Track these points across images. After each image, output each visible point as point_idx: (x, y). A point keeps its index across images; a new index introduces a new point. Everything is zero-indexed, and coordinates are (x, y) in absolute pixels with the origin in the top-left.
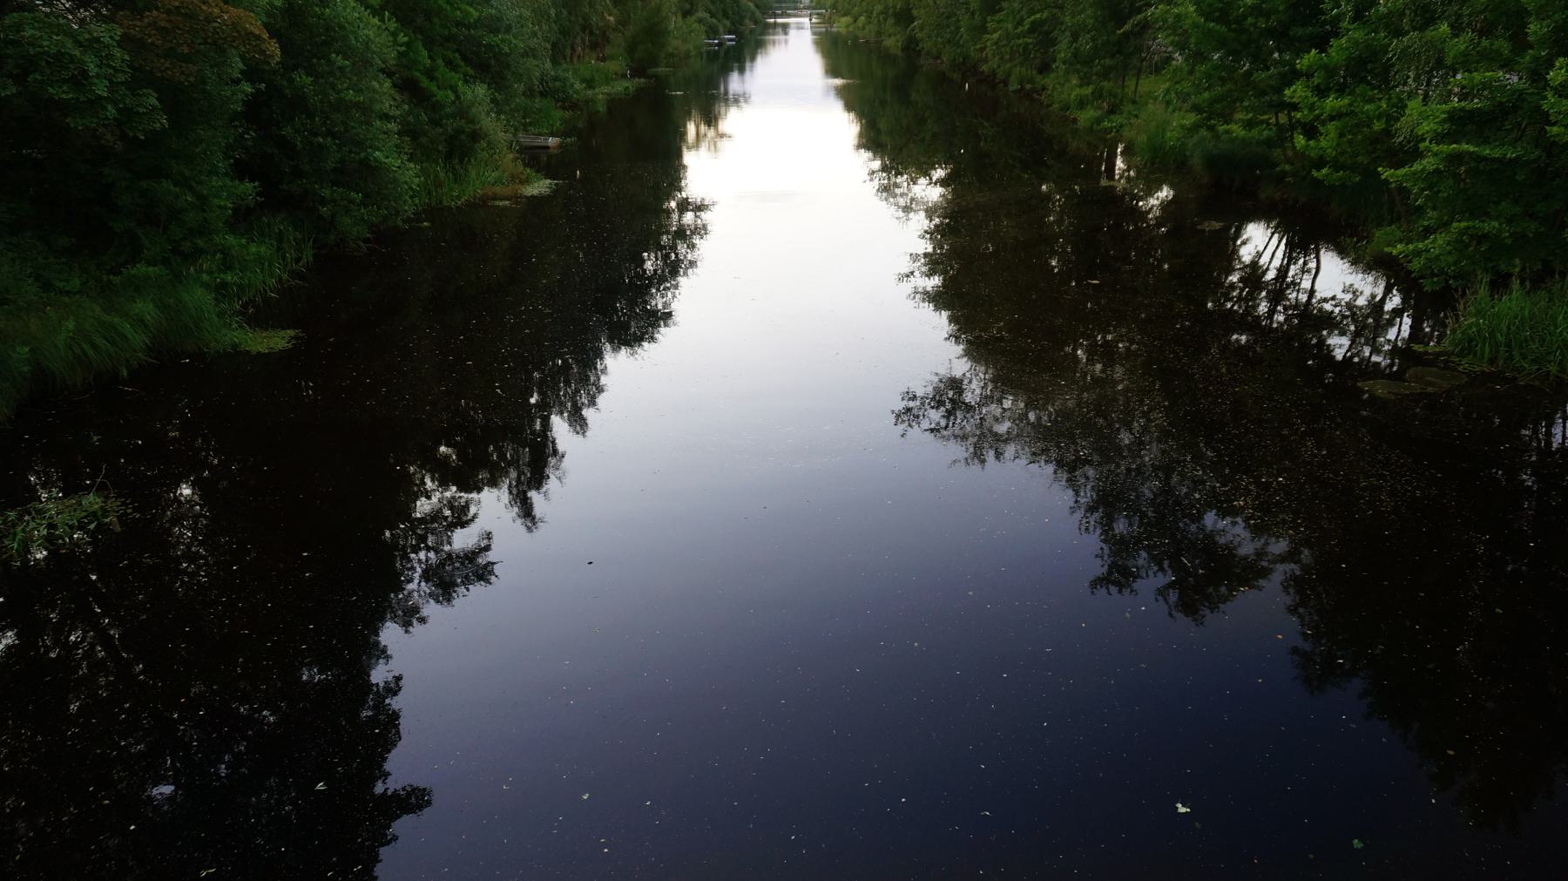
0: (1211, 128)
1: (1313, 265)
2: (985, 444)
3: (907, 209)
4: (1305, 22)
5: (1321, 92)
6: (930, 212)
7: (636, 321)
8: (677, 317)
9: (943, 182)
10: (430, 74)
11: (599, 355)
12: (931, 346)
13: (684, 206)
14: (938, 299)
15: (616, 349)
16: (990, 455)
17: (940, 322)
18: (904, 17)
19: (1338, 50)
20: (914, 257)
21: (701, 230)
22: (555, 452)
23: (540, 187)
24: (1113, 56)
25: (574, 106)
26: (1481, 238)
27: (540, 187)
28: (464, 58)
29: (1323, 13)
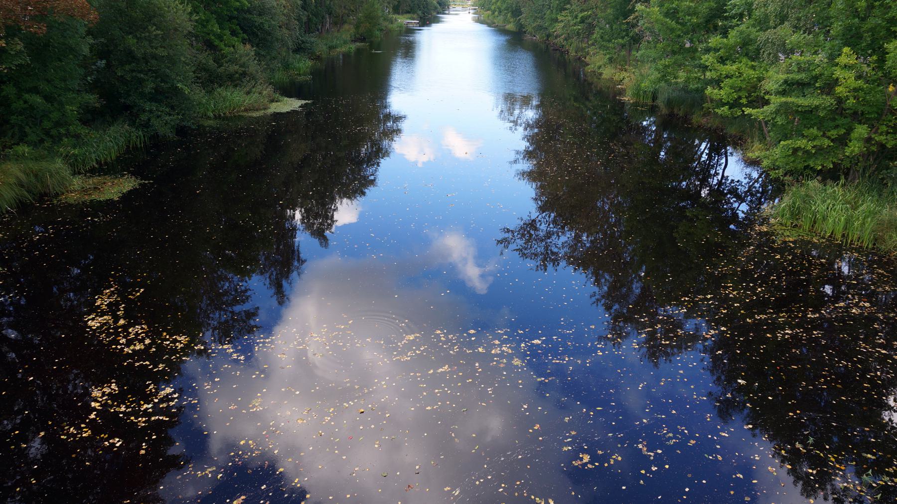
0: (666, 81)
1: (723, 161)
2: (549, 258)
3: (515, 123)
4: (715, 20)
5: (722, 61)
6: (528, 126)
7: (357, 184)
8: (379, 182)
9: (538, 107)
10: (220, 38)
11: (333, 200)
12: (522, 200)
13: (388, 116)
14: (531, 176)
15: (341, 198)
16: (550, 266)
17: (528, 190)
18: (516, 12)
19: (733, 36)
20: (518, 152)
21: (398, 131)
22: (299, 259)
23: (293, 104)
24: (623, 38)
25: (318, 58)
26: (796, 150)
27: (293, 104)
28: (242, 28)
29: (726, 11)
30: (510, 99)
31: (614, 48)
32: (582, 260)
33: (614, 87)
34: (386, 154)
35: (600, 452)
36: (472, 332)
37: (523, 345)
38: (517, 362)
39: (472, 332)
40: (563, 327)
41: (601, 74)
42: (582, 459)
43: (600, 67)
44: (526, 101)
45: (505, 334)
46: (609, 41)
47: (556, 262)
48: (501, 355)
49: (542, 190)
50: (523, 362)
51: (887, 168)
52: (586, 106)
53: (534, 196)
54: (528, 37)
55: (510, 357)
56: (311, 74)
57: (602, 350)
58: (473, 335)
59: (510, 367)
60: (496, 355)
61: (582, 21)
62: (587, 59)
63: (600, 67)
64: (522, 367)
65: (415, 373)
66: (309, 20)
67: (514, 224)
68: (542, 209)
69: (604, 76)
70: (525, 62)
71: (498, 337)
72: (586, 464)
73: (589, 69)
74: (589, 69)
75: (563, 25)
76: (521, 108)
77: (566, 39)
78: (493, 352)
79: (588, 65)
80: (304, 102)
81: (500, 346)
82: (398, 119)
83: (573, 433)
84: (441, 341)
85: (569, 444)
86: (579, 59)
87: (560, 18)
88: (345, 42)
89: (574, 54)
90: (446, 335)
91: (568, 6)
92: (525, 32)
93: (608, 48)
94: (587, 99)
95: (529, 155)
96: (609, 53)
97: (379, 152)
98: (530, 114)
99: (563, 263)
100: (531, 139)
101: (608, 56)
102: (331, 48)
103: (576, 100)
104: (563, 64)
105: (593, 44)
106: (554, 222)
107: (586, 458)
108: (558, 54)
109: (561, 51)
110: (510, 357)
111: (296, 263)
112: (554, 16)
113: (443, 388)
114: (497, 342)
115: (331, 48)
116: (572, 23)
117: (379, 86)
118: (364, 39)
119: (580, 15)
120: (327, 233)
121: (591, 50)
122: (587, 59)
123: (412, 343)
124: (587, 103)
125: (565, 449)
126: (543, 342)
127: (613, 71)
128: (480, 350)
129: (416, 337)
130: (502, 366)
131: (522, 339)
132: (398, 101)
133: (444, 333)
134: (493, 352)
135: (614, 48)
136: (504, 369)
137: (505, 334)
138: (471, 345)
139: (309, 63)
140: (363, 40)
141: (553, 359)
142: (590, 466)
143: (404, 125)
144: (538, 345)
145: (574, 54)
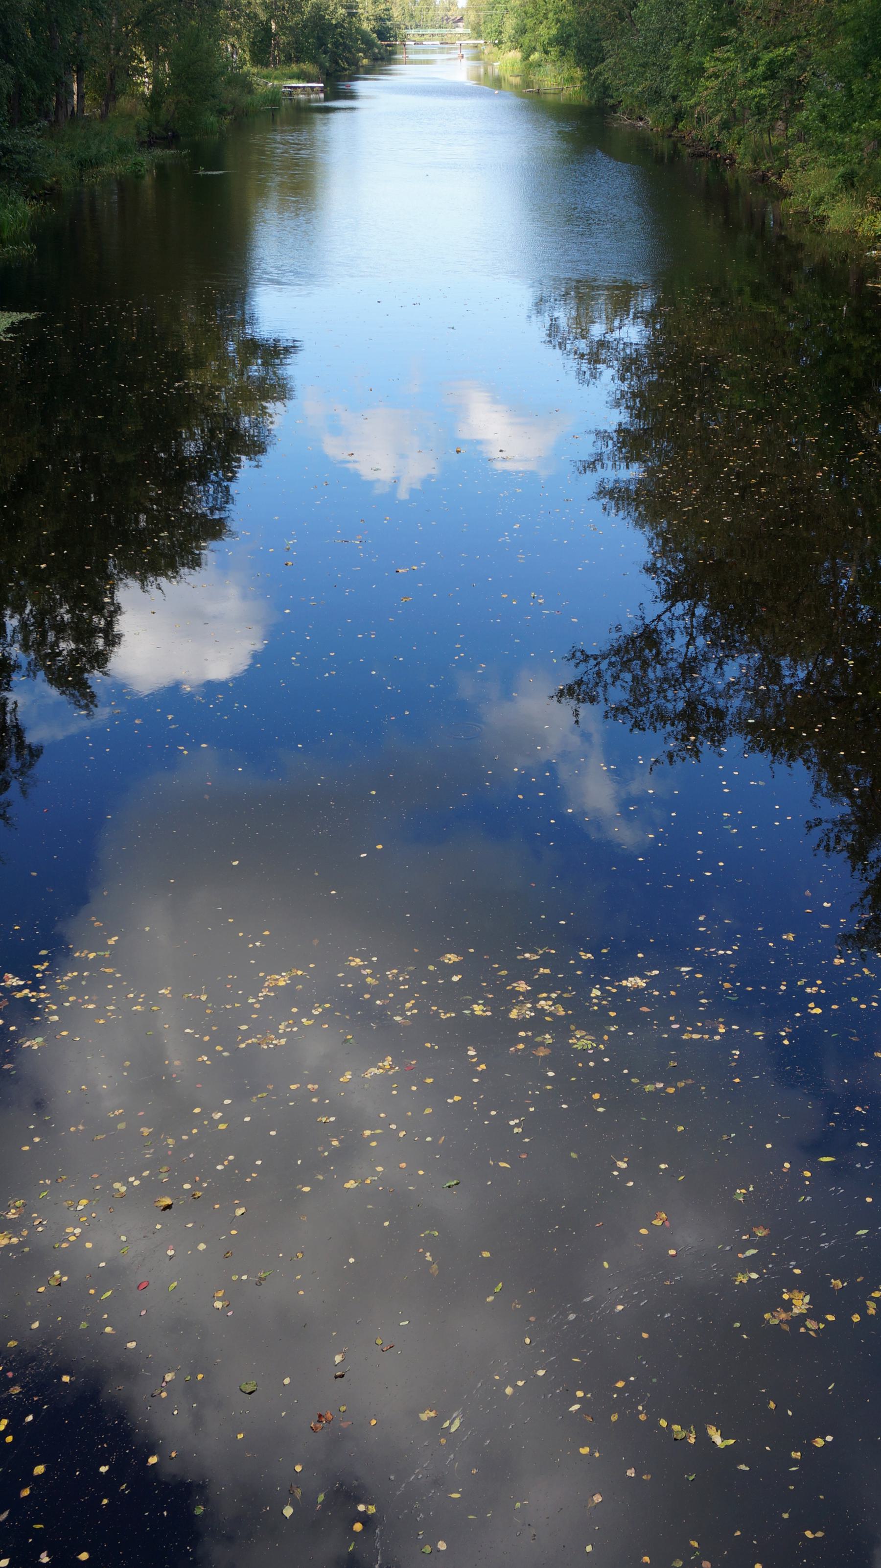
2: (700, 722)
3: (594, 358)
6: (629, 365)
8: (232, 525)
12: (616, 569)
14: (196, 563)
17: (629, 543)
25: (51, 194)
30: (581, 293)
31: (858, 146)
32: (776, 735)
33: (859, 257)
34: (256, 448)
35: (837, 1284)
36: (451, 958)
37: (596, 992)
38: (581, 1041)
39: (451, 958)
40: (704, 940)
41: (822, 220)
42: (788, 1306)
43: (819, 201)
44: (621, 301)
45: (544, 961)
46: (843, 128)
47: (717, 734)
48: (538, 1023)
49: (668, 543)
50: (599, 1041)
51: (691, 756)
52: (783, 310)
53: (646, 556)
54: (622, 120)
55: (561, 1028)
56: (34, 238)
57: (818, 1000)
58: (455, 968)
59: (562, 1056)
60: (523, 1024)
61: (771, 74)
62: (785, 180)
63: (819, 201)
64: (598, 1055)
65: (304, 1084)
66: (21, 89)
67: (598, 642)
68: (672, 595)
69: (831, 225)
70: (614, 186)
71: (525, 971)
72: (800, 1319)
73: (792, 205)
74: (792, 205)
75: (715, 87)
76: (610, 320)
77: (725, 125)
78: (514, 1014)
79: (786, 194)
80: (17, 317)
81: (533, 997)
82: (274, 352)
83: (761, 1233)
84: (367, 988)
85: (751, 1264)
86: (764, 178)
87: (709, 65)
88: (123, 149)
89: (748, 165)
90: (378, 970)
91: (732, 32)
92: (614, 108)
93: (840, 147)
94: (788, 288)
95: (631, 443)
96: (843, 162)
97: (234, 444)
98: (633, 333)
99: (735, 743)
100: (642, 402)
101: (841, 170)
102: (85, 164)
103: (757, 292)
104: (720, 195)
105: (799, 138)
106: (706, 627)
107: (801, 1303)
108: (704, 167)
109: (715, 158)
110: (561, 1028)
111: (13, 763)
112: (694, 58)
113: (385, 1124)
114: (522, 986)
115: (85, 164)
116: (741, 79)
117: (218, 263)
118: (175, 136)
119: (767, 57)
120: (95, 677)
121: (797, 153)
122: (785, 180)
123: (287, 995)
124: (787, 302)
125: (742, 1279)
126: (653, 983)
127: (856, 211)
128: (478, 1009)
129: (295, 980)
130: (542, 1052)
131: (598, 971)
132: (273, 309)
133: (371, 965)
134: (514, 1014)
135: (858, 146)
136: (548, 1061)
137: (544, 961)
138: (454, 997)
139: (27, 209)
140: (170, 139)
141: (682, 1031)
142: (811, 1324)
143: (294, 370)
144: (637, 990)
145: (748, 165)
